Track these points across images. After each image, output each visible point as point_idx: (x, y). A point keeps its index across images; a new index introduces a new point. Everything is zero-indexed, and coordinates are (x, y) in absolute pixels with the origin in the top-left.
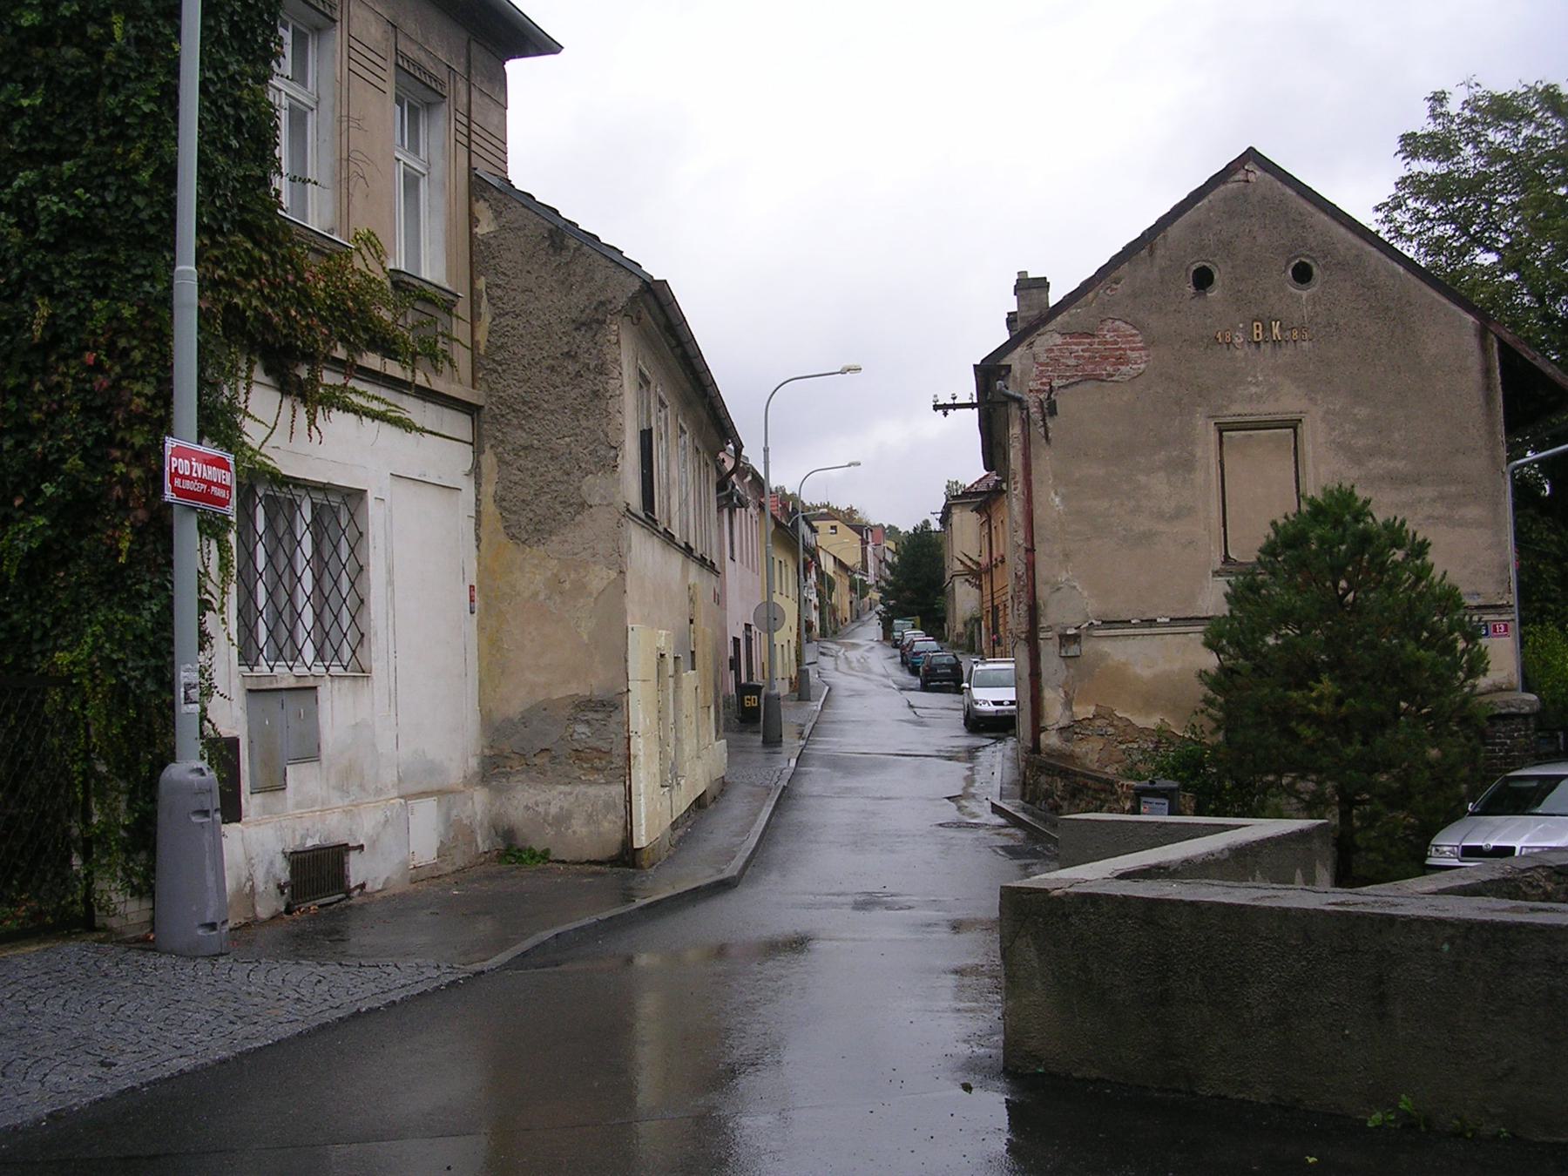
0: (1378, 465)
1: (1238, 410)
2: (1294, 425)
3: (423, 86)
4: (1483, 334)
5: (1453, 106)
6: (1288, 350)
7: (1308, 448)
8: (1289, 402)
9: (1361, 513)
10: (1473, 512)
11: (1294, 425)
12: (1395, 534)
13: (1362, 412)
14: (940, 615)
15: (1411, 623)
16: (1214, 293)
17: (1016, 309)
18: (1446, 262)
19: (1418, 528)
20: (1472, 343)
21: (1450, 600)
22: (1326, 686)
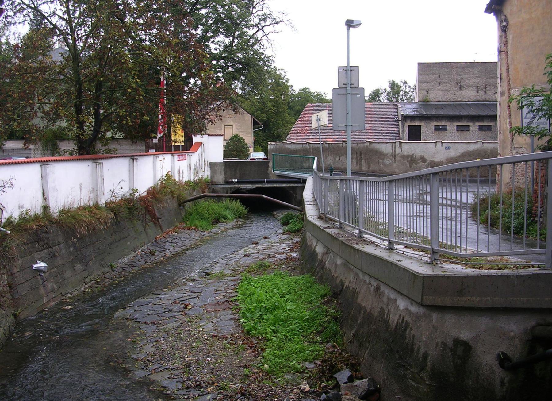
0: (240, 130)
1: (227, 124)
2: (232, 126)
3: (503, 172)
4: (251, 117)
5: (137, 195)
6: (232, 118)
7: (233, 128)
8: (231, 124)
9: (239, 136)
10: (250, 135)
11: (232, 126)
12: (242, 138)
13: (239, 125)
14: (124, 210)
15: (243, 147)
16: (225, 112)
17: (492, 56)
18: (58, 36)
19: (244, 138)
20: (250, 118)
21: (246, 144)
22: (236, 152)
